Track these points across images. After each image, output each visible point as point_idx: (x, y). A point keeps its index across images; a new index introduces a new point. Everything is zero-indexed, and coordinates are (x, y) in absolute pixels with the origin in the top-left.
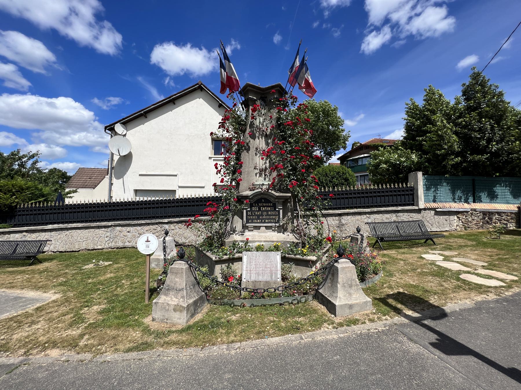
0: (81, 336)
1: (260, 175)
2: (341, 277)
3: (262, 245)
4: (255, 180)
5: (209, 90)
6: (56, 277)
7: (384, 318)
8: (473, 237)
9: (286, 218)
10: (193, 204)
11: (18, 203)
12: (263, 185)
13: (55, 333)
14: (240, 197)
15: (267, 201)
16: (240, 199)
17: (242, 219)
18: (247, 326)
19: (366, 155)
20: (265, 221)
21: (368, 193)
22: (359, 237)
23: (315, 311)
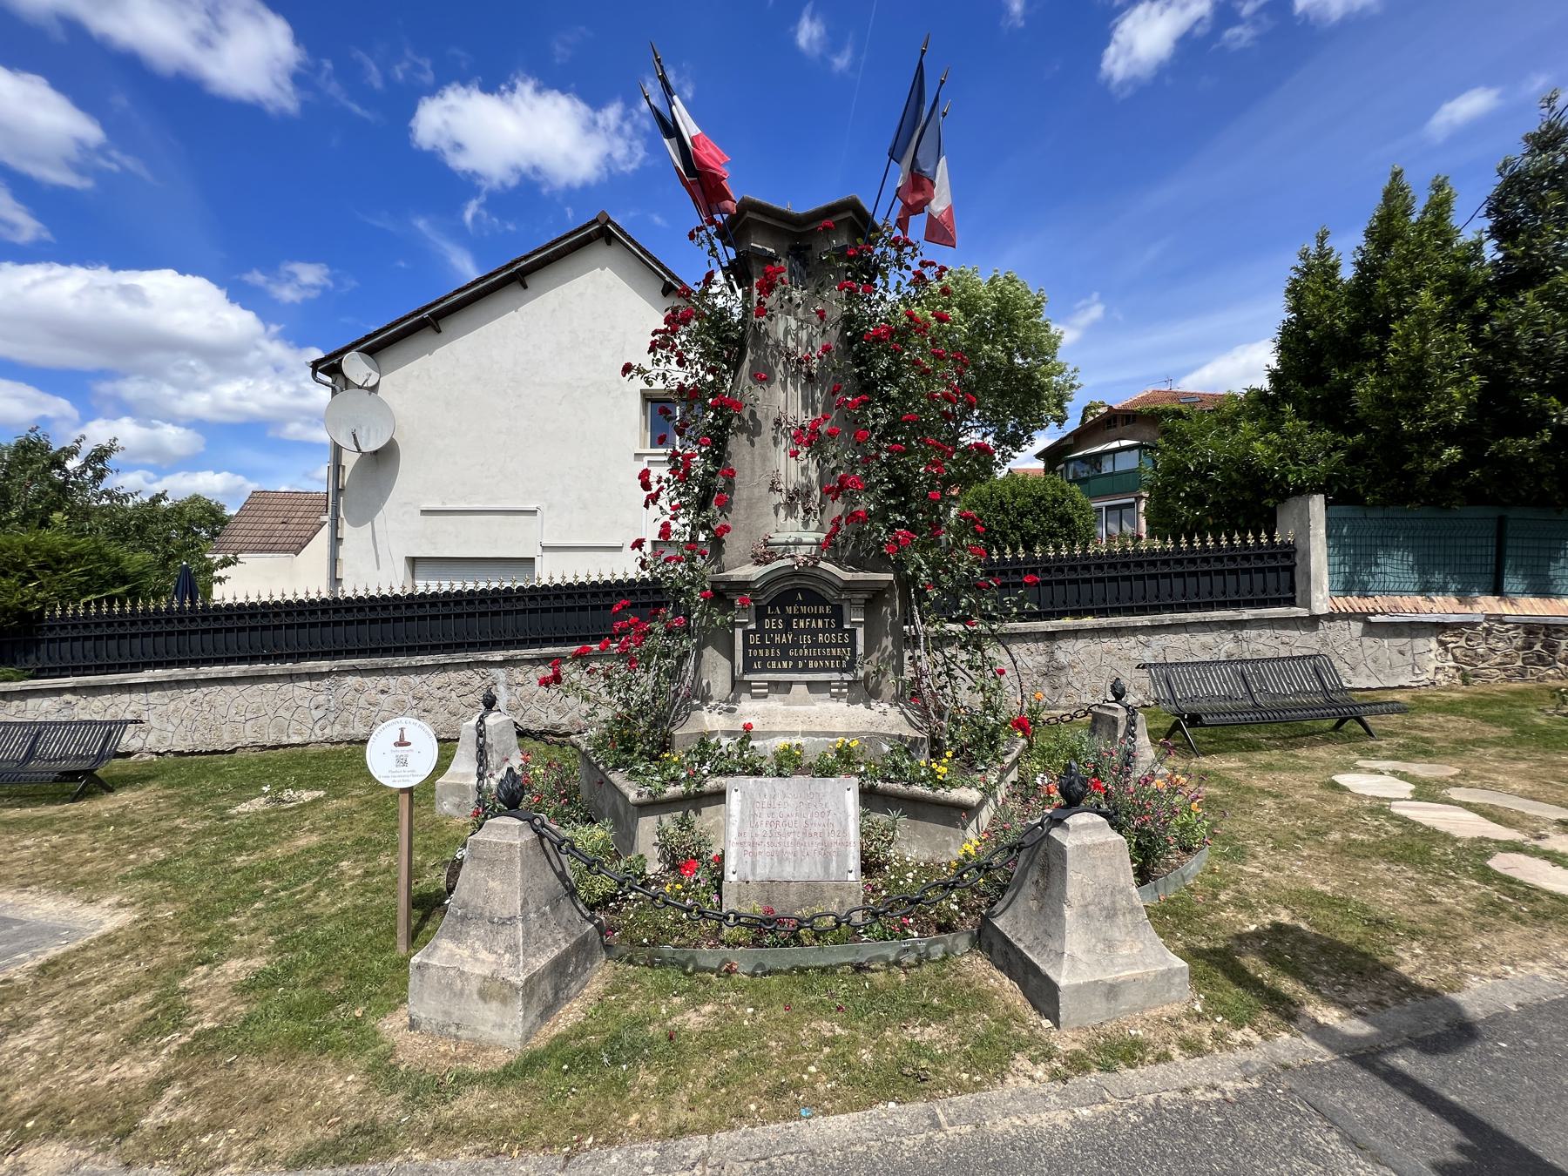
0: (157, 1087)
2: (1078, 881)
3: (798, 745)
5: (632, 241)
6: (140, 844)
7: (1238, 1036)
8: (1496, 711)
9: (876, 655)
11: (44, 602)
12: (798, 543)
13: (75, 1073)
14: (723, 587)
15: (813, 598)
16: (723, 594)
17: (731, 658)
18: (738, 1061)
19: (1125, 443)
21: (1142, 567)
22: (1121, 715)
23: (982, 1000)
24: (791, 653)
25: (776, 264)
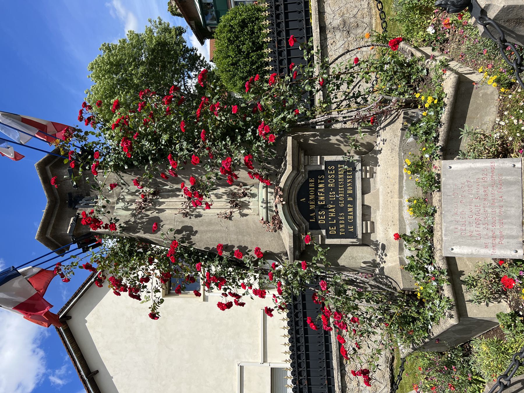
1: (245, 205)
4: (256, 217)
5: (69, 303)
9: (342, 147)
10: (302, 340)
14: (297, 253)
17: (346, 246)
20: (350, 195)
24: (342, 205)
25: (81, 216)
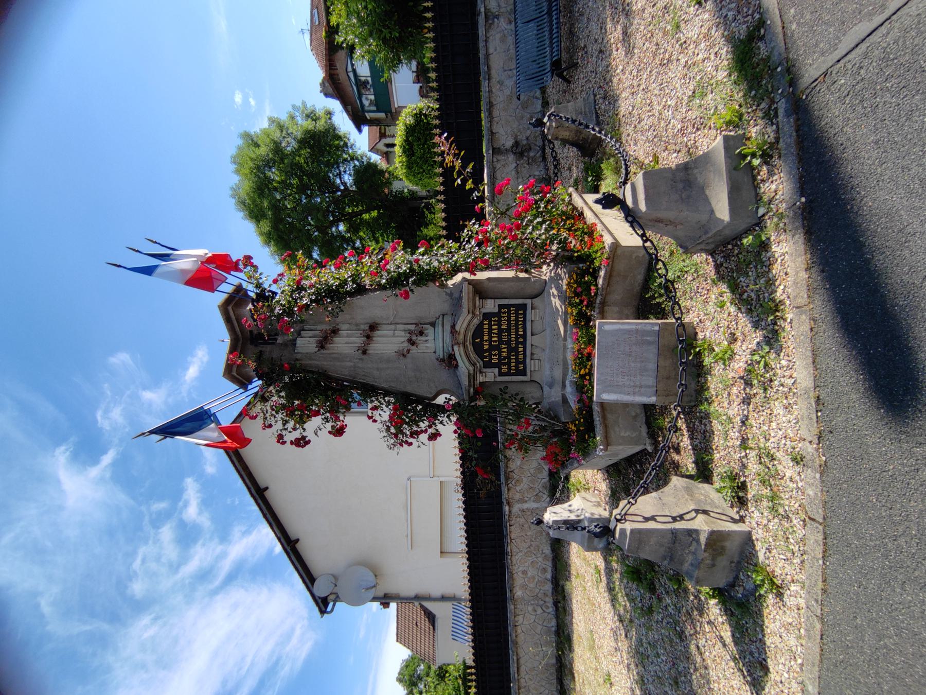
14: (472, 390)
